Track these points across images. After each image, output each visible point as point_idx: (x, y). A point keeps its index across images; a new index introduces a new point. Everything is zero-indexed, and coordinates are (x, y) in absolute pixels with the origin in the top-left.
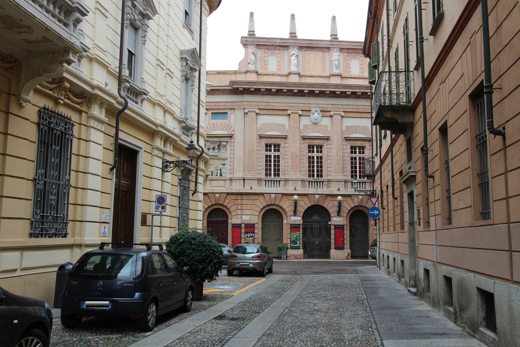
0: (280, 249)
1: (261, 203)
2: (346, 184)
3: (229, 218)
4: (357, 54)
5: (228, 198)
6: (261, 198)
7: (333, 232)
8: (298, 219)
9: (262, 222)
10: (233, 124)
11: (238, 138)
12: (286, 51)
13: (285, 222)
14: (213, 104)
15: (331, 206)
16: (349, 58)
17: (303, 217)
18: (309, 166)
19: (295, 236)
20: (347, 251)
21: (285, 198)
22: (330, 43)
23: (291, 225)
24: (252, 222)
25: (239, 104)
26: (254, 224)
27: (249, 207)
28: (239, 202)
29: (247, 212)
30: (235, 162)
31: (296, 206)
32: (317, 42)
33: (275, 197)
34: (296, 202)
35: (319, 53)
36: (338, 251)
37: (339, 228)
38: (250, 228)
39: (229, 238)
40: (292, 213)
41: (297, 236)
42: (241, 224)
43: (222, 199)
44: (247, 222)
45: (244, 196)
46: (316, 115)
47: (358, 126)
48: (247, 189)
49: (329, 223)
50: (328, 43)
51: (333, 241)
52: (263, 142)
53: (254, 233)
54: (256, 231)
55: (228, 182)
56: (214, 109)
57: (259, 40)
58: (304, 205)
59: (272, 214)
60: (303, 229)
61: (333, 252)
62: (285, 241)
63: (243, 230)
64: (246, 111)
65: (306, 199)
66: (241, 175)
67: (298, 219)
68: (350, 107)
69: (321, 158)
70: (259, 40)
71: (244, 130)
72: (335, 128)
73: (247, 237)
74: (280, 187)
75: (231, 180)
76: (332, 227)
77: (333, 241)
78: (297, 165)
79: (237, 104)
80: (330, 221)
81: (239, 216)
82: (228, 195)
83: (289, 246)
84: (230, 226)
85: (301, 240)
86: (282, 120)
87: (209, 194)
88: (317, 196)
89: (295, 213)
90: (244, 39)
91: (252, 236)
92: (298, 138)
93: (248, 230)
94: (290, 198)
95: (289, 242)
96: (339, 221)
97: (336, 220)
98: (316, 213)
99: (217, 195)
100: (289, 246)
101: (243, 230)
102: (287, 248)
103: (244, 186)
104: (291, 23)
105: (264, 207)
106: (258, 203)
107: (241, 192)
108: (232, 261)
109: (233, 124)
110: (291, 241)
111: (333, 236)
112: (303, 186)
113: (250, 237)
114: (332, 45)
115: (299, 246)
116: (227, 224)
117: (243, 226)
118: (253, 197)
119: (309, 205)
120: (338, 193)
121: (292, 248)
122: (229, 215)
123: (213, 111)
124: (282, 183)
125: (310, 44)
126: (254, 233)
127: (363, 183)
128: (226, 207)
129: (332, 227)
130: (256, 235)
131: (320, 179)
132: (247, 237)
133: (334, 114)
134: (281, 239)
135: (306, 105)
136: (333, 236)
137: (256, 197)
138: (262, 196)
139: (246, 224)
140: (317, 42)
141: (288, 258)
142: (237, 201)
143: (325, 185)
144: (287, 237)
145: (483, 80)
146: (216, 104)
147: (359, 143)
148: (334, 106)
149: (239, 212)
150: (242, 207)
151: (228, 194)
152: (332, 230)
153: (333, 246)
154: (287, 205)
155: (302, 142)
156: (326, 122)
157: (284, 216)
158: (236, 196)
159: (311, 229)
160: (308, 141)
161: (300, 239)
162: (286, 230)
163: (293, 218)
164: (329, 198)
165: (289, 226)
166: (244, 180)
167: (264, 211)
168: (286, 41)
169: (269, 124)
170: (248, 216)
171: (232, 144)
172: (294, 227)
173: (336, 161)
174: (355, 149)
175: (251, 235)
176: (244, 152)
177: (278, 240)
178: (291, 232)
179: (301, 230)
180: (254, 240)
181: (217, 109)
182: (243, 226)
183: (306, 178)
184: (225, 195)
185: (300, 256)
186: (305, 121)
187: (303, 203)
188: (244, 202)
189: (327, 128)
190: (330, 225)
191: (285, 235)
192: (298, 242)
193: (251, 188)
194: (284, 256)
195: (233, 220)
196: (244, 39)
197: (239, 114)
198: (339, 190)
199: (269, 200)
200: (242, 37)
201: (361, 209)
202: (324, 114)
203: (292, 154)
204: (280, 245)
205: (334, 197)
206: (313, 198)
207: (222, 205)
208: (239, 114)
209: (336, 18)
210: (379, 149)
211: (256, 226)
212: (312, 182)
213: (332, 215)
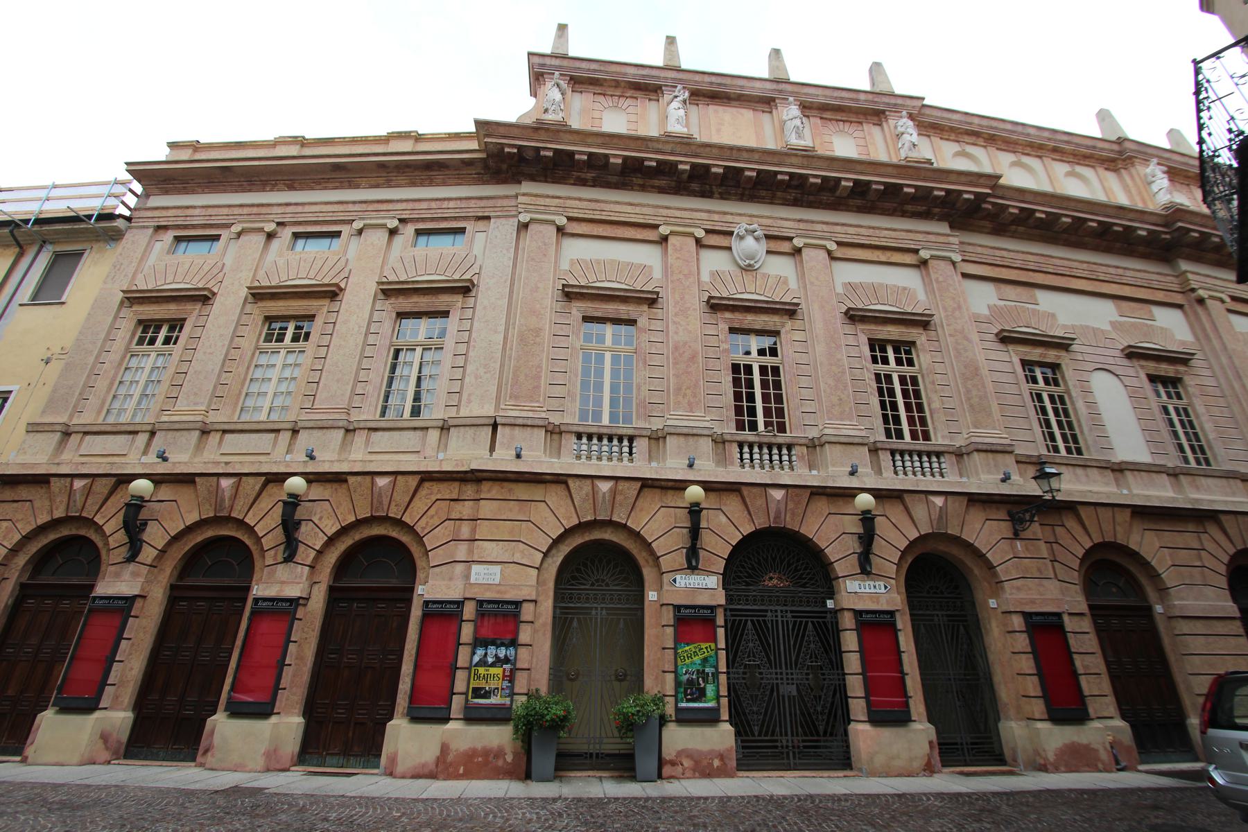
0: (629, 726)
1: (553, 516)
2: (350, 435)
4: (847, 125)
5: (423, 492)
6: (554, 496)
7: (850, 641)
8: (705, 587)
9: (559, 596)
10: (480, 257)
11: (490, 296)
12: (653, 104)
13: (652, 596)
14: (424, 205)
15: (832, 534)
16: (826, 131)
17: (730, 577)
18: (737, 396)
19: (697, 659)
20: (921, 732)
21: (651, 502)
22: (774, 86)
23: (677, 608)
25: (505, 202)
26: (518, 604)
27: (503, 530)
28: (466, 509)
29: (492, 550)
30: (469, 369)
31: (695, 532)
32: (741, 82)
33: (614, 492)
34: (695, 511)
35: (744, 111)
36: (886, 733)
37: (875, 625)
38: (501, 619)
39: (404, 668)
40: (680, 559)
41: (705, 660)
42: (460, 604)
43: (401, 497)
44: (489, 596)
45: (486, 486)
46: (750, 241)
47: (881, 285)
48: (503, 460)
49: (830, 604)
50: (769, 86)
51: (855, 686)
52: (574, 311)
53: (514, 643)
54: (524, 635)
55: (434, 435)
56: (423, 220)
57: (577, 64)
58: (727, 528)
59: (599, 567)
60: (726, 627)
61: (863, 734)
62: (649, 682)
63: (467, 632)
64: (524, 218)
65: (732, 505)
66: (489, 410)
67: (705, 587)
68: (851, 230)
69: (776, 370)
70: (577, 64)
71: (513, 274)
72: (812, 283)
73: (482, 663)
74: (631, 460)
75: (445, 428)
76: (847, 621)
77: (855, 686)
78: (696, 385)
79: (499, 203)
80: (831, 594)
81: (459, 568)
82: (427, 484)
83: (670, 710)
84: (416, 613)
85: (723, 679)
86: (647, 256)
87: (351, 480)
88: (778, 494)
89: (693, 560)
90: (536, 60)
91: (507, 660)
92: (696, 304)
93: (486, 632)
94: (671, 498)
95: (669, 688)
96: (874, 597)
97: (861, 592)
98: (777, 559)
99: (382, 482)
100: (670, 710)
101: (467, 632)
102: (663, 721)
103: (492, 449)
104: (666, 49)
105: (568, 533)
106: (540, 514)
107: (474, 466)
110: (678, 683)
111: (853, 663)
112: (723, 460)
113: (498, 662)
114: (780, 91)
115: (716, 710)
116: (409, 601)
117: (469, 611)
118: (522, 491)
119: (747, 529)
120: (854, 483)
121: (685, 718)
122: (420, 563)
123: (421, 226)
124: (641, 445)
125: (720, 84)
126: (514, 643)
127: (780, 447)
128: (411, 529)
129: (847, 621)
130: (523, 653)
131: (781, 439)
132: (482, 663)
133: (806, 245)
134: (632, 676)
135: (716, 217)
136: (853, 663)
137: (537, 492)
138: (560, 489)
139: (481, 603)
140: (741, 82)
141: (667, 770)
142: (458, 506)
143: (801, 458)
144: (662, 663)
146: (433, 205)
147: (893, 332)
148: (802, 226)
149: (461, 552)
150: (474, 530)
151: (427, 477)
153: (858, 707)
154: (658, 525)
155: (709, 318)
156: (781, 267)
157: (648, 573)
158: (456, 484)
159: (761, 629)
160: (728, 315)
161: (716, 675)
162: (658, 633)
164: (822, 506)
165: (668, 616)
166: (495, 426)
167: (565, 549)
168: (654, 73)
169: (598, 262)
170: (497, 569)
171: (469, 313)
172: (691, 621)
173: (828, 382)
174: (883, 350)
175: (502, 652)
176: (505, 338)
177: (621, 678)
178: (679, 639)
179: (721, 632)
180: (511, 678)
181: (433, 219)
182: (469, 611)
183: (730, 429)
184: (413, 482)
185: (721, 757)
186: (713, 261)
187: (724, 519)
188: (487, 509)
189: (786, 282)
190: (835, 612)
191: (650, 653)
192: (710, 690)
193: (518, 456)
194: (645, 763)
195: (433, 587)
196: (536, 60)
197: (503, 229)
198: (852, 473)
199: (588, 505)
200: (530, 54)
201: (942, 547)
202: (775, 246)
203: (676, 348)
204: (629, 706)
205: (840, 502)
206: (760, 502)
207: (399, 523)
208: (503, 229)
209: (783, 52)
211: (527, 612)
212: (751, 446)
213: (840, 569)
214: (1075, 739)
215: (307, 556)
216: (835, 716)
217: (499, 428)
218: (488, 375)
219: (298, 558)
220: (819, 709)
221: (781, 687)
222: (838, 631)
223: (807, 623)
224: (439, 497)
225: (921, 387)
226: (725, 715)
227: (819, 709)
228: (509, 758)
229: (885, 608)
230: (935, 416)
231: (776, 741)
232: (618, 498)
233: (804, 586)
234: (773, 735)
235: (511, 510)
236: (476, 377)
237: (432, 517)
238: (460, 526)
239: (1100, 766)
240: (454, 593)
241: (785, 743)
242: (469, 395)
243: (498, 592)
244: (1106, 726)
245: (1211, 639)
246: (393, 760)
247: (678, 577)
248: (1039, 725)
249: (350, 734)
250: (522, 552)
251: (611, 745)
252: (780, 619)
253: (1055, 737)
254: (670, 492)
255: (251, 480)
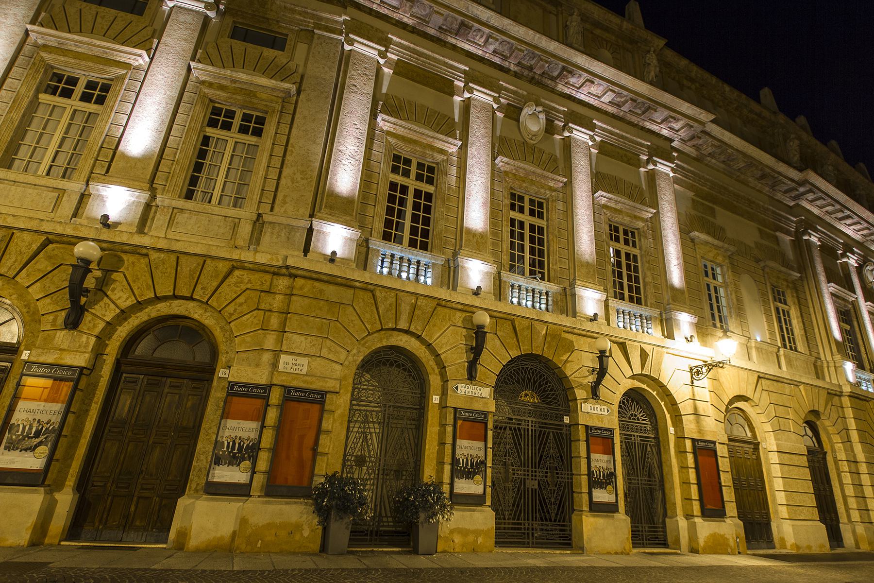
3: (223, 359)
8: (479, 394)
24: (317, 385)
49: (567, 420)
67: (479, 394)
96: (600, 417)
108: (648, 124)
109: (302, 64)
117: (275, 396)
119: (515, 353)
145: (714, 217)
152: (723, 476)
163: (465, 389)
170: (304, 361)
172: (471, 422)
199: (391, 315)
210: (106, 513)
211: (331, 401)
214: (717, 531)
215: (95, 326)
216: (563, 508)
217: (267, 229)
218: (305, 182)
219: (83, 327)
220: (553, 500)
221: (527, 481)
222: (571, 441)
223: (549, 433)
224: (249, 286)
225: (639, 265)
226: (488, 503)
227: (553, 500)
228: (306, 533)
229: (606, 426)
230: (648, 287)
231: (521, 524)
232: (417, 312)
233: (549, 404)
234: (518, 519)
235: (320, 309)
236: (293, 181)
237: (241, 305)
238: (270, 317)
239: (729, 550)
240: (261, 377)
241: (527, 526)
242: (285, 196)
243: (304, 382)
244: (730, 527)
245: (791, 468)
246: (183, 535)
247: (460, 386)
248: (697, 520)
249: (133, 508)
250: (329, 349)
251: (388, 524)
252: (530, 428)
253: (705, 529)
254: (800, 320)
255: (27, 236)
